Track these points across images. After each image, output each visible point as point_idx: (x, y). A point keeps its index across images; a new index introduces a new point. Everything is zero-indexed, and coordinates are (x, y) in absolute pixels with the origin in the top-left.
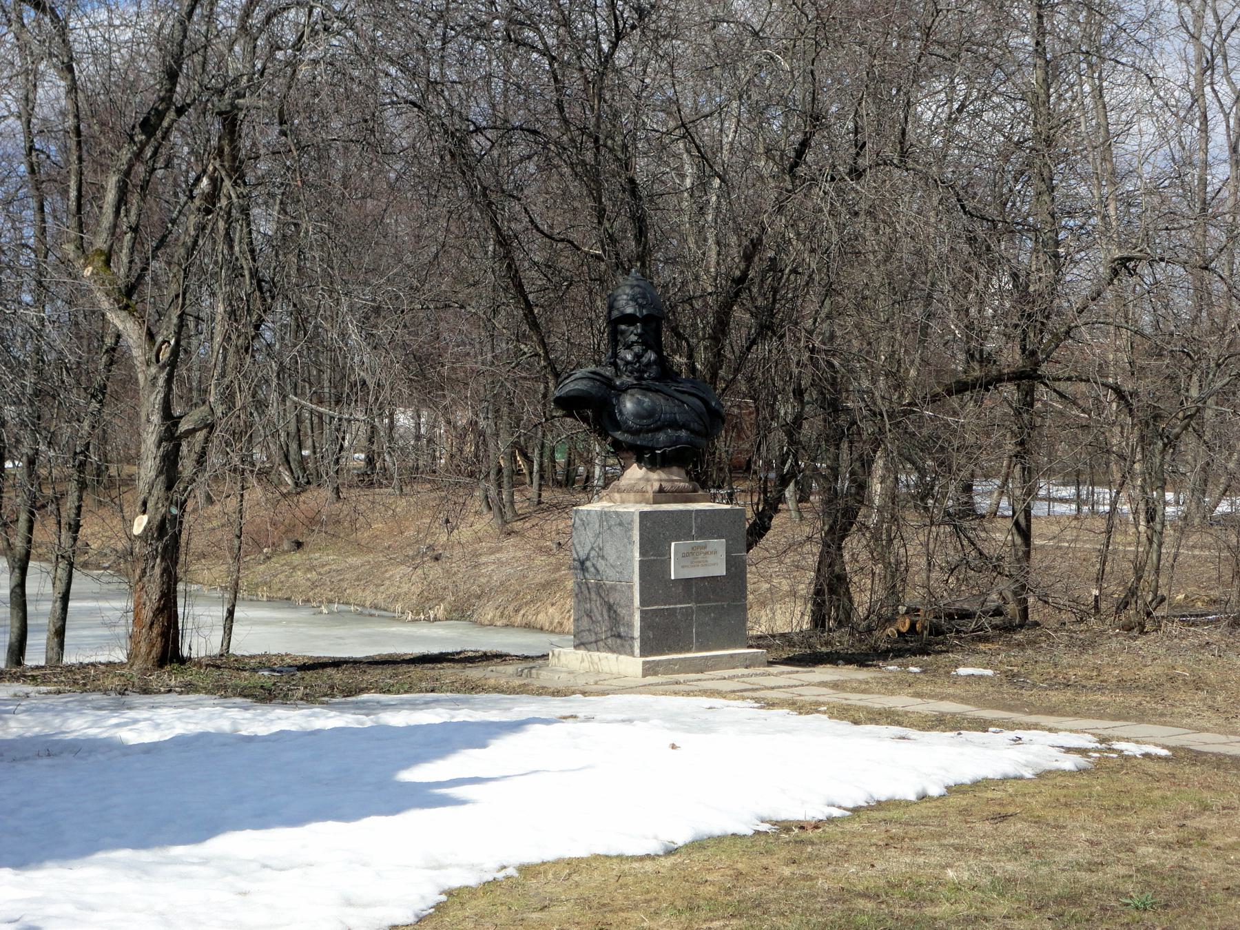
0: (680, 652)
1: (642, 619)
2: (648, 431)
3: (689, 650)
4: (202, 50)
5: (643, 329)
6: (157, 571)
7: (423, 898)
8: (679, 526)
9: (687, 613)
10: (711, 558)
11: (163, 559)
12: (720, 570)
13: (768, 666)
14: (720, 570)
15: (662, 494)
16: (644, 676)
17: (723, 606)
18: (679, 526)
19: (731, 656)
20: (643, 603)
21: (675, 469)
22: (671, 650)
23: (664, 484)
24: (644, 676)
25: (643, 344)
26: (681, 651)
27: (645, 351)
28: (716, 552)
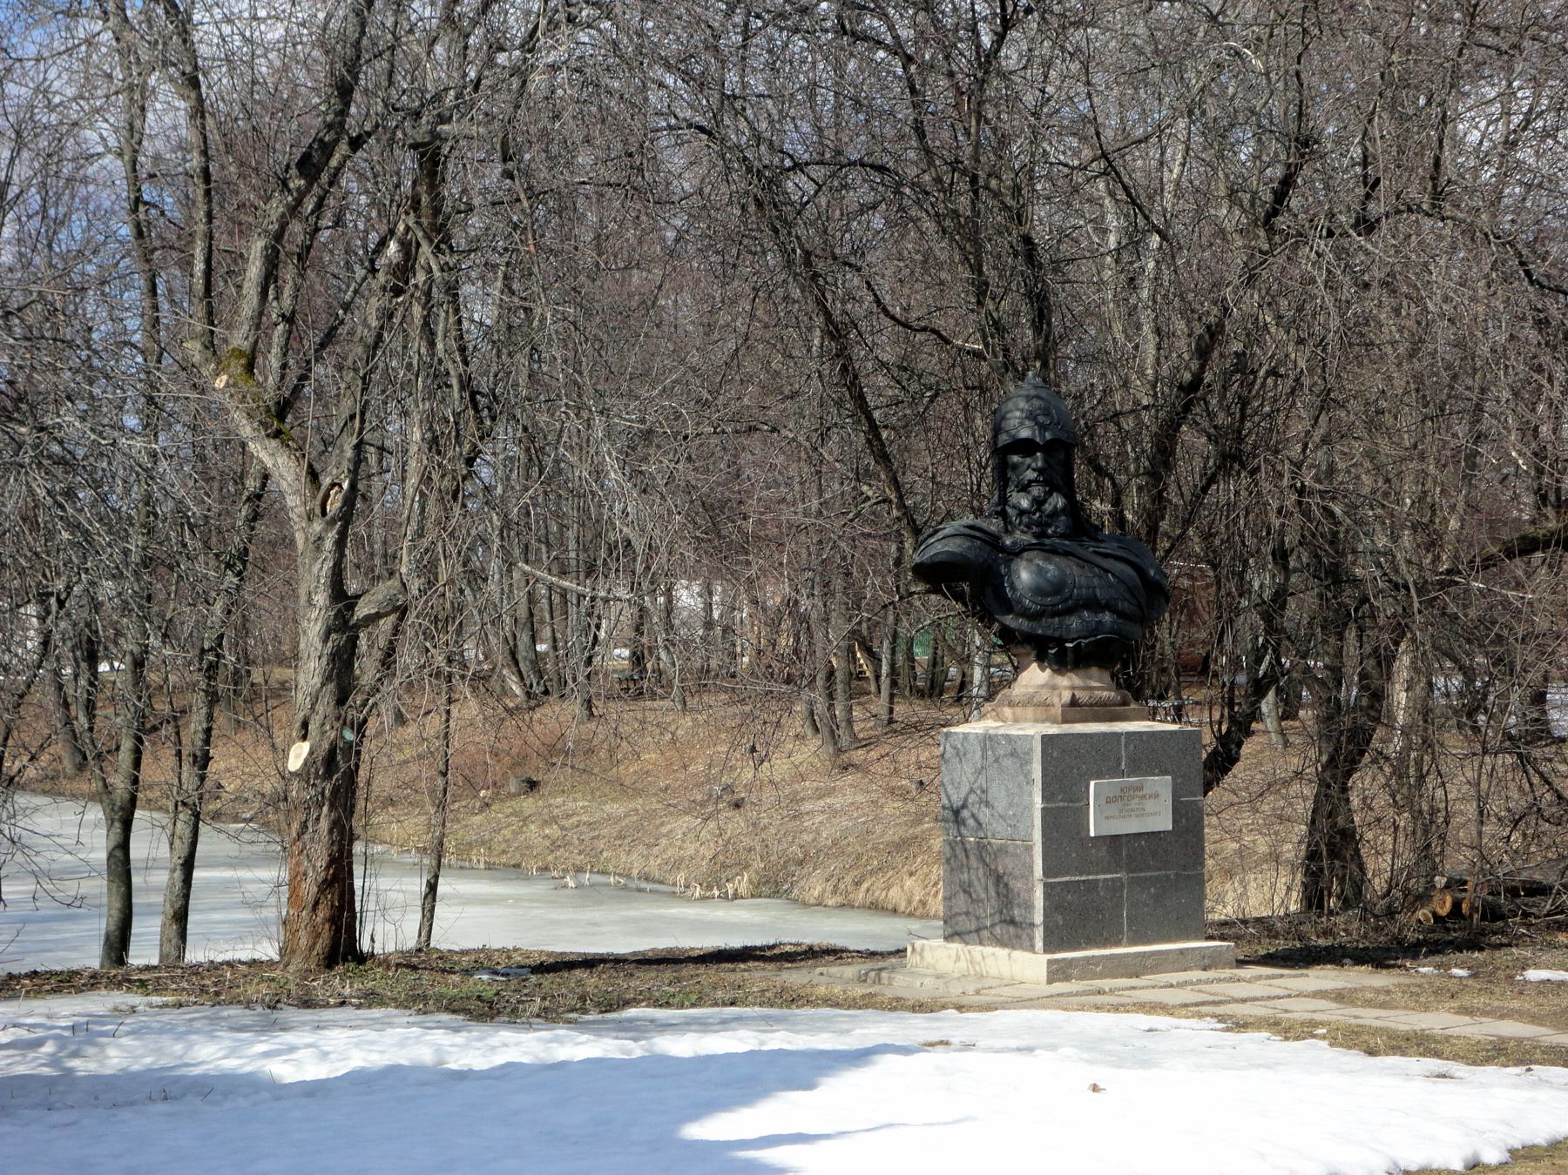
2: (1054, 615)
3: (1118, 943)
5: (1046, 461)
6: (324, 825)
9: (1115, 886)
10: (1150, 805)
12: (1163, 822)
13: (1237, 967)
14: (1163, 822)
16: (1050, 982)
17: (1167, 877)
19: (1182, 952)
21: (1094, 671)
22: (1090, 942)
23: (1078, 694)
24: (1050, 982)
25: (1045, 483)
26: (1105, 943)
27: (1049, 494)
28: (1157, 796)
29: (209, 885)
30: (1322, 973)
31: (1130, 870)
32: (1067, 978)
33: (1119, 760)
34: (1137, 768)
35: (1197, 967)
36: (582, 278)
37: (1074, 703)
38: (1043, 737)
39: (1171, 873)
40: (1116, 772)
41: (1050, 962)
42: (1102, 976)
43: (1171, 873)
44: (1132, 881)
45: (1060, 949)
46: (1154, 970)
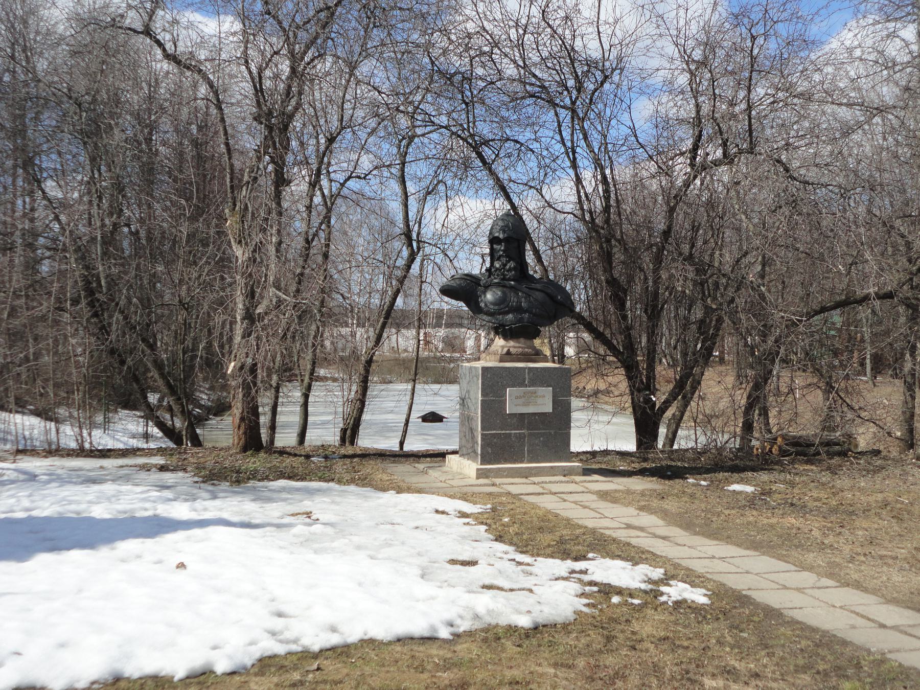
0: (514, 463)
1: (482, 439)
2: (500, 314)
3: (522, 462)
4: (464, 18)
5: (505, 246)
6: (241, 396)
7: (477, 617)
8: (516, 378)
9: (521, 437)
10: (540, 401)
11: (243, 389)
12: (548, 408)
13: (584, 475)
14: (548, 408)
15: (508, 356)
16: (478, 478)
17: (550, 434)
18: (516, 378)
19: (552, 467)
20: (482, 429)
21: (522, 340)
22: (506, 461)
23: (511, 350)
24: (478, 478)
25: (507, 256)
26: (515, 462)
27: (509, 261)
28: (544, 396)
29: (315, 424)
30: (637, 481)
31: (528, 429)
32: (487, 477)
33: (525, 379)
34: (533, 383)
35: (560, 475)
36: (836, 363)
37: (508, 353)
38: (483, 368)
39: (552, 432)
40: (522, 384)
41: (478, 470)
42: (507, 477)
43: (552, 432)
44: (530, 435)
45: (490, 462)
46: (536, 475)
